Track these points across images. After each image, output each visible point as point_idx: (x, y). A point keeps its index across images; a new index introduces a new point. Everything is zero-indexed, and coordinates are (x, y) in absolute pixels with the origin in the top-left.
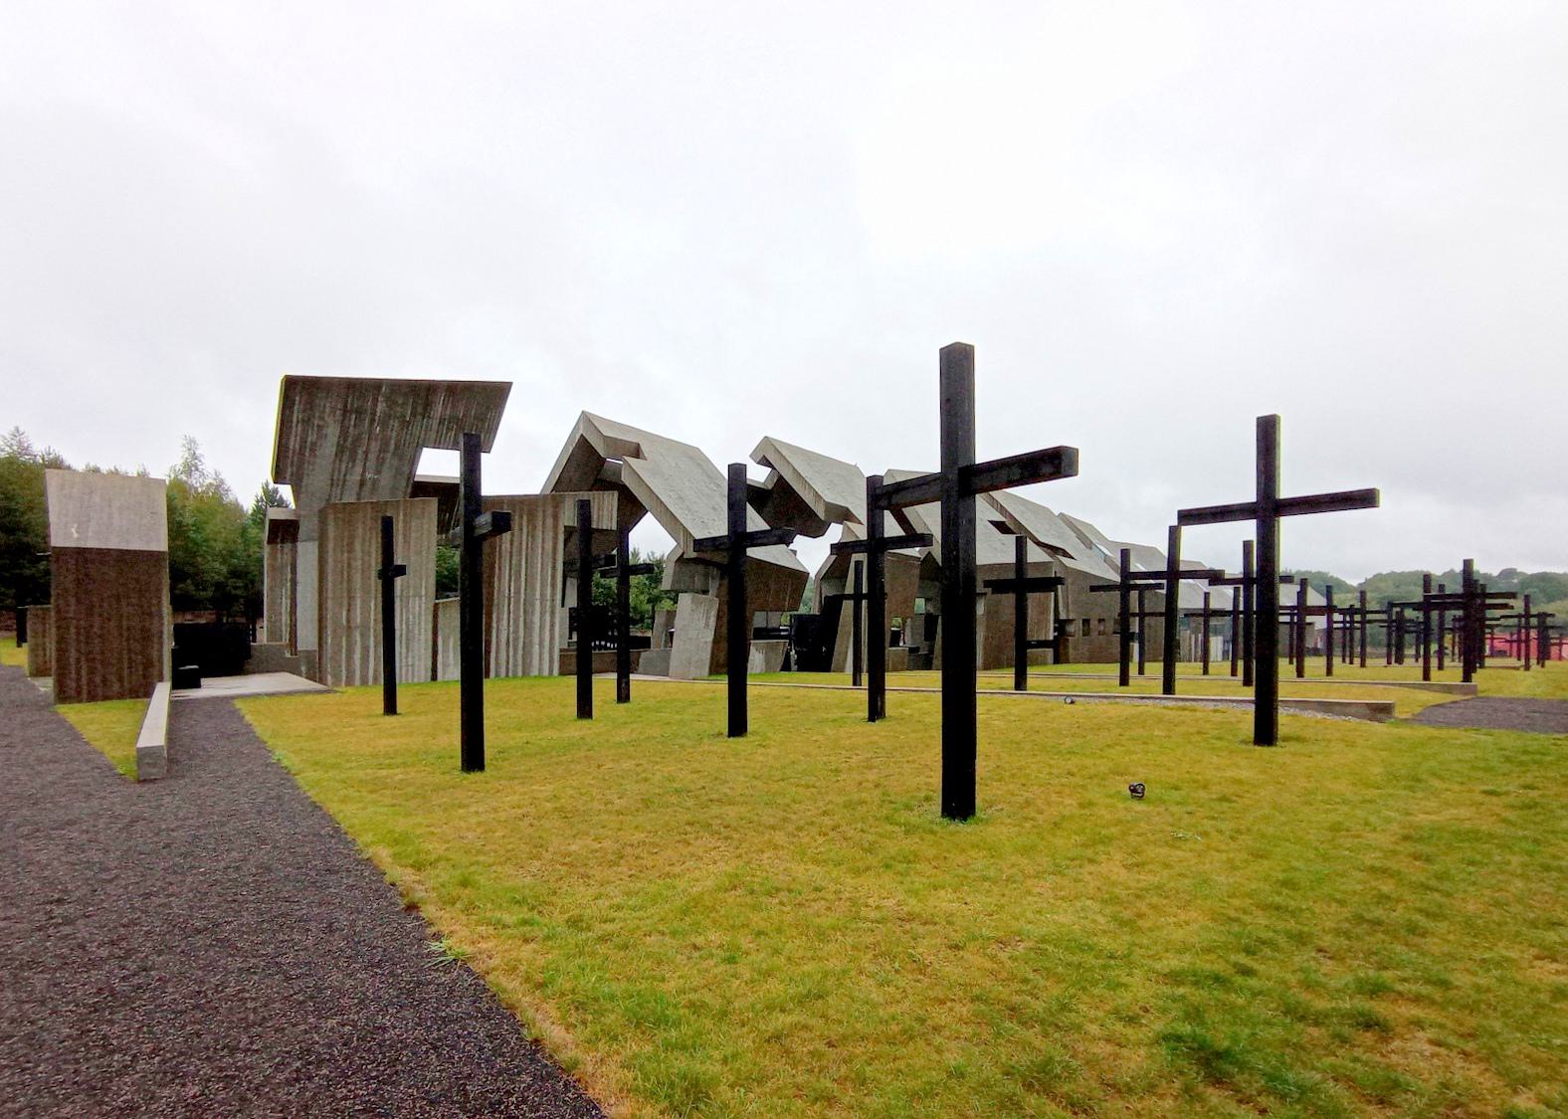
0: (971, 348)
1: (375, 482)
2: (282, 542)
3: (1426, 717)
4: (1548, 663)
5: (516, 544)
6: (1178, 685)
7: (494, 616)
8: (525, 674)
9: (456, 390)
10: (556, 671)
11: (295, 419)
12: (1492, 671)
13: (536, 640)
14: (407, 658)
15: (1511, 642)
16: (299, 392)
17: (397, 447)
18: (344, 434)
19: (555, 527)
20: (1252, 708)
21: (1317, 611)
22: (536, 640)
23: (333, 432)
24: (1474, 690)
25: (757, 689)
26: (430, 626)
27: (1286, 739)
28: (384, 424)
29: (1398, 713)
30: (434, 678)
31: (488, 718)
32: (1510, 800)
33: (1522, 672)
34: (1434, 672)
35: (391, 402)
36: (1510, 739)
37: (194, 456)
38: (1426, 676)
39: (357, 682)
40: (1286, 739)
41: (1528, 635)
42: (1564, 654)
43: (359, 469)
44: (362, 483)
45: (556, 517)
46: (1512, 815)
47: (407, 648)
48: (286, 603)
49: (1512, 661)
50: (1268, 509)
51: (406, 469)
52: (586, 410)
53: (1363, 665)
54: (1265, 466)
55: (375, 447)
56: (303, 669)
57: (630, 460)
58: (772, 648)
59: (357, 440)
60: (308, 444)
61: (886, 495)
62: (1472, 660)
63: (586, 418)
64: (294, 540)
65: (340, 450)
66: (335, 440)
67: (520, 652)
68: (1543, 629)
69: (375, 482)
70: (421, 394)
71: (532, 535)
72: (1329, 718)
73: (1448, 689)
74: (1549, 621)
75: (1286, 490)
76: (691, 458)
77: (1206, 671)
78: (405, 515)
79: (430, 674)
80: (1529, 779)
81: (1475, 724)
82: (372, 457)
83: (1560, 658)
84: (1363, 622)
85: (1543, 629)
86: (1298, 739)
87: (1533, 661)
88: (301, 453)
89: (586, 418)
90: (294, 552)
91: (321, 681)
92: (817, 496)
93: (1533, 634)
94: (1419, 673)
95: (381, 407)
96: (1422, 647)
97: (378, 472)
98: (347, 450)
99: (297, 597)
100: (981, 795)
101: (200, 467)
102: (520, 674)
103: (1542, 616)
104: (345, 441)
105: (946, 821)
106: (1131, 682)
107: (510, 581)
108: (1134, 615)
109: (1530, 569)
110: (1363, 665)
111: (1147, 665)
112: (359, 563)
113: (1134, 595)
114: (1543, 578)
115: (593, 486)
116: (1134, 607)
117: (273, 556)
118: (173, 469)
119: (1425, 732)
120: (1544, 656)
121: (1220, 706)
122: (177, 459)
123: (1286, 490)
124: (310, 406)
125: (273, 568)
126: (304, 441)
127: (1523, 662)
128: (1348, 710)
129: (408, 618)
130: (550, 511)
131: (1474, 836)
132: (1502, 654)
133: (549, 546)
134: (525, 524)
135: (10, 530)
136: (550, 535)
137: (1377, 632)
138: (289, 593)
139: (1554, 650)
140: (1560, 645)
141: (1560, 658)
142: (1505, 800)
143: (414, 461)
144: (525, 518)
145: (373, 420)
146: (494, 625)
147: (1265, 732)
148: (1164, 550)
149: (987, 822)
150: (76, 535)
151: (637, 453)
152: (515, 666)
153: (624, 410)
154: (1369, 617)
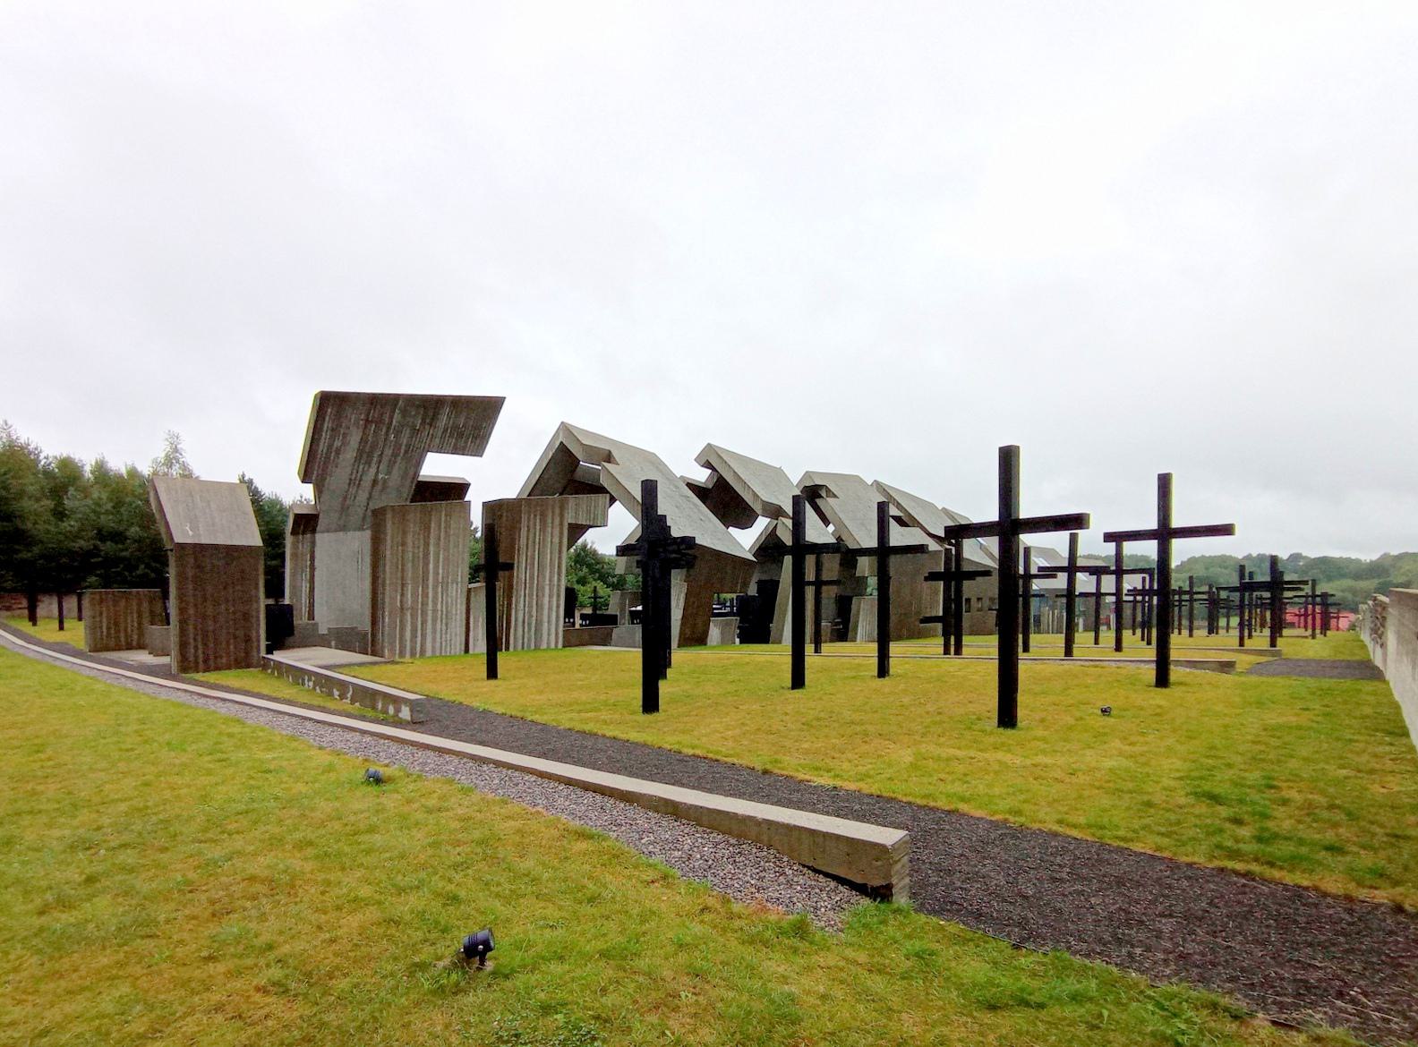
0: (1017, 448)
1: (385, 481)
2: (303, 533)
3: (1255, 670)
4: (1329, 633)
5: (531, 540)
6: (1076, 652)
7: (514, 599)
8: (537, 647)
9: (458, 403)
10: (560, 646)
11: (325, 428)
12: (1290, 640)
13: (545, 619)
14: (446, 633)
15: (1300, 616)
16: (330, 406)
17: (406, 452)
18: (363, 441)
19: (561, 524)
20: (1154, 666)
21: (1071, 582)
22: (545, 619)
23: (355, 438)
24: (1278, 653)
25: (1102, 635)
26: (464, 607)
27: (1174, 684)
28: (398, 433)
29: (1239, 668)
30: (467, 650)
31: (993, 646)
32: (1316, 712)
33: (1310, 640)
34: (1247, 641)
35: (404, 413)
36: (1311, 682)
37: (176, 450)
38: (1242, 644)
39: (201, 665)
40: (1174, 684)
41: (1314, 610)
42: (1340, 626)
43: (373, 470)
44: (375, 482)
45: (562, 516)
46: (1319, 719)
47: (447, 625)
48: (305, 587)
49: (1301, 631)
50: (1164, 534)
51: (411, 473)
52: (571, 421)
53: (1191, 635)
54: (1163, 507)
55: (388, 452)
56: (333, 643)
57: (605, 464)
58: (727, 624)
59: (373, 447)
60: (334, 449)
61: (958, 532)
62: (1277, 629)
63: (565, 428)
64: (314, 531)
65: (360, 452)
66: (356, 446)
67: (533, 629)
68: (1325, 605)
69: (385, 481)
70: (430, 406)
71: (543, 529)
72: (1193, 670)
73: (1260, 652)
74: (1330, 600)
75: (1176, 523)
76: (652, 463)
77: (1096, 642)
78: (446, 515)
79: (463, 648)
80: (1326, 702)
81: (1288, 674)
82: (385, 460)
83: (1338, 629)
84: (1191, 601)
85: (1325, 605)
86: (1181, 684)
87: (1318, 631)
88: (327, 457)
89: (565, 428)
90: (313, 543)
91: (374, 654)
92: (755, 495)
93: (1318, 609)
94: (1237, 641)
95: (397, 416)
96: (952, 638)
97: (389, 473)
98: (365, 454)
99: (333, 578)
100: (1021, 713)
101: (181, 460)
102: (533, 647)
103: (1324, 596)
104: (364, 447)
105: (1001, 730)
106: (1031, 649)
107: (526, 568)
108: (810, 583)
109: (1313, 553)
110: (1191, 635)
111: (895, 648)
112: (410, 555)
113: (810, 561)
114: (1324, 561)
115: (565, 488)
116: (810, 575)
117: (295, 546)
118: (155, 461)
119: (1254, 679)
120: (1325, 627)
121: (1121, 664)
122: (161, 454)
123: (1176, 523)
124: (339, 416)
125: (294, 555)
126: (330, 446)
127: (1309, 632)
128: (1206, 665)
129: (447, 603)
130: (557, 511)
131: (1299, 728)
132: (1292, 625)
133: (556, 540)
134: (538, 524)
135: (9, 517)
136: (557, 531)
137: (1200, 609)
138: (308, 577)
139: (1333, 622)
140: (1338, 618)
141: (1338, 629)
142: (1313, 712)
143: (419, 464)
144: (538, 517)
145: (388, 428)
146: (513, 606)
147: (1162, 680)
148: (1065, 554)
149: (1022, 729)
150: (191, 533)
151: (609, 458)
152: (529, 640)
153: (602, 421)
154: (1196, 597)
